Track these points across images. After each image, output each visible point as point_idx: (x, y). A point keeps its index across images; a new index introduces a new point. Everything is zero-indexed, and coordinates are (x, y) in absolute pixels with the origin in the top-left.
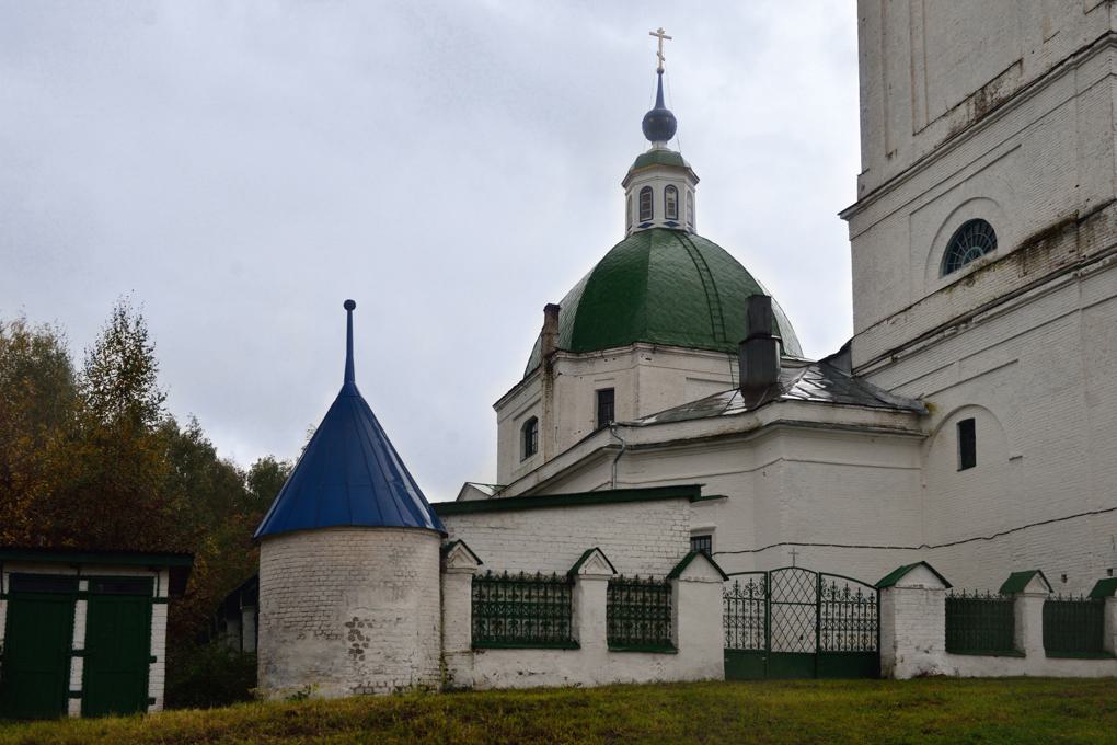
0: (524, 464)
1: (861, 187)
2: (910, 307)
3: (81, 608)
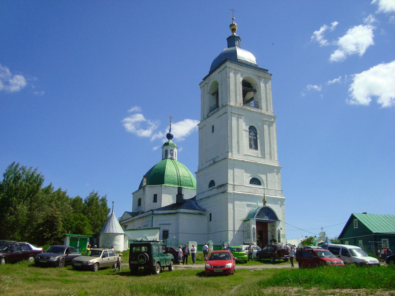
0: (138, 207)
1: (198, 169)
2: (204, 192)
3: (79, 242)
